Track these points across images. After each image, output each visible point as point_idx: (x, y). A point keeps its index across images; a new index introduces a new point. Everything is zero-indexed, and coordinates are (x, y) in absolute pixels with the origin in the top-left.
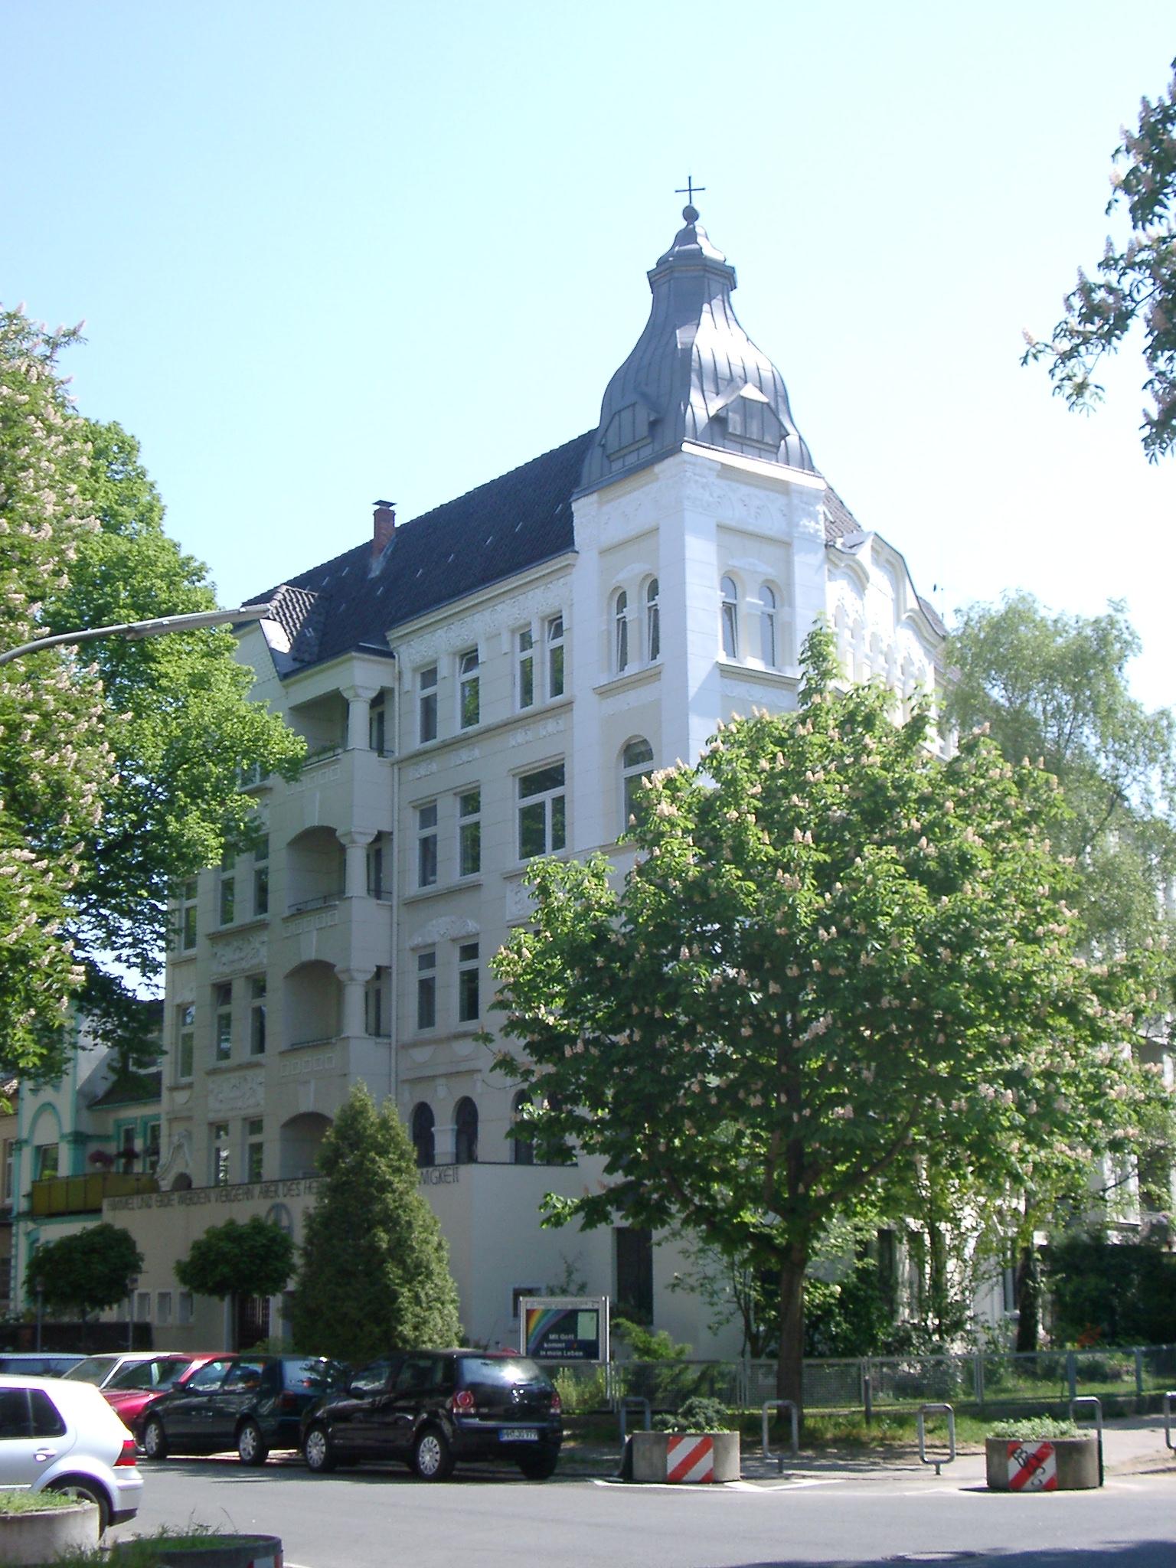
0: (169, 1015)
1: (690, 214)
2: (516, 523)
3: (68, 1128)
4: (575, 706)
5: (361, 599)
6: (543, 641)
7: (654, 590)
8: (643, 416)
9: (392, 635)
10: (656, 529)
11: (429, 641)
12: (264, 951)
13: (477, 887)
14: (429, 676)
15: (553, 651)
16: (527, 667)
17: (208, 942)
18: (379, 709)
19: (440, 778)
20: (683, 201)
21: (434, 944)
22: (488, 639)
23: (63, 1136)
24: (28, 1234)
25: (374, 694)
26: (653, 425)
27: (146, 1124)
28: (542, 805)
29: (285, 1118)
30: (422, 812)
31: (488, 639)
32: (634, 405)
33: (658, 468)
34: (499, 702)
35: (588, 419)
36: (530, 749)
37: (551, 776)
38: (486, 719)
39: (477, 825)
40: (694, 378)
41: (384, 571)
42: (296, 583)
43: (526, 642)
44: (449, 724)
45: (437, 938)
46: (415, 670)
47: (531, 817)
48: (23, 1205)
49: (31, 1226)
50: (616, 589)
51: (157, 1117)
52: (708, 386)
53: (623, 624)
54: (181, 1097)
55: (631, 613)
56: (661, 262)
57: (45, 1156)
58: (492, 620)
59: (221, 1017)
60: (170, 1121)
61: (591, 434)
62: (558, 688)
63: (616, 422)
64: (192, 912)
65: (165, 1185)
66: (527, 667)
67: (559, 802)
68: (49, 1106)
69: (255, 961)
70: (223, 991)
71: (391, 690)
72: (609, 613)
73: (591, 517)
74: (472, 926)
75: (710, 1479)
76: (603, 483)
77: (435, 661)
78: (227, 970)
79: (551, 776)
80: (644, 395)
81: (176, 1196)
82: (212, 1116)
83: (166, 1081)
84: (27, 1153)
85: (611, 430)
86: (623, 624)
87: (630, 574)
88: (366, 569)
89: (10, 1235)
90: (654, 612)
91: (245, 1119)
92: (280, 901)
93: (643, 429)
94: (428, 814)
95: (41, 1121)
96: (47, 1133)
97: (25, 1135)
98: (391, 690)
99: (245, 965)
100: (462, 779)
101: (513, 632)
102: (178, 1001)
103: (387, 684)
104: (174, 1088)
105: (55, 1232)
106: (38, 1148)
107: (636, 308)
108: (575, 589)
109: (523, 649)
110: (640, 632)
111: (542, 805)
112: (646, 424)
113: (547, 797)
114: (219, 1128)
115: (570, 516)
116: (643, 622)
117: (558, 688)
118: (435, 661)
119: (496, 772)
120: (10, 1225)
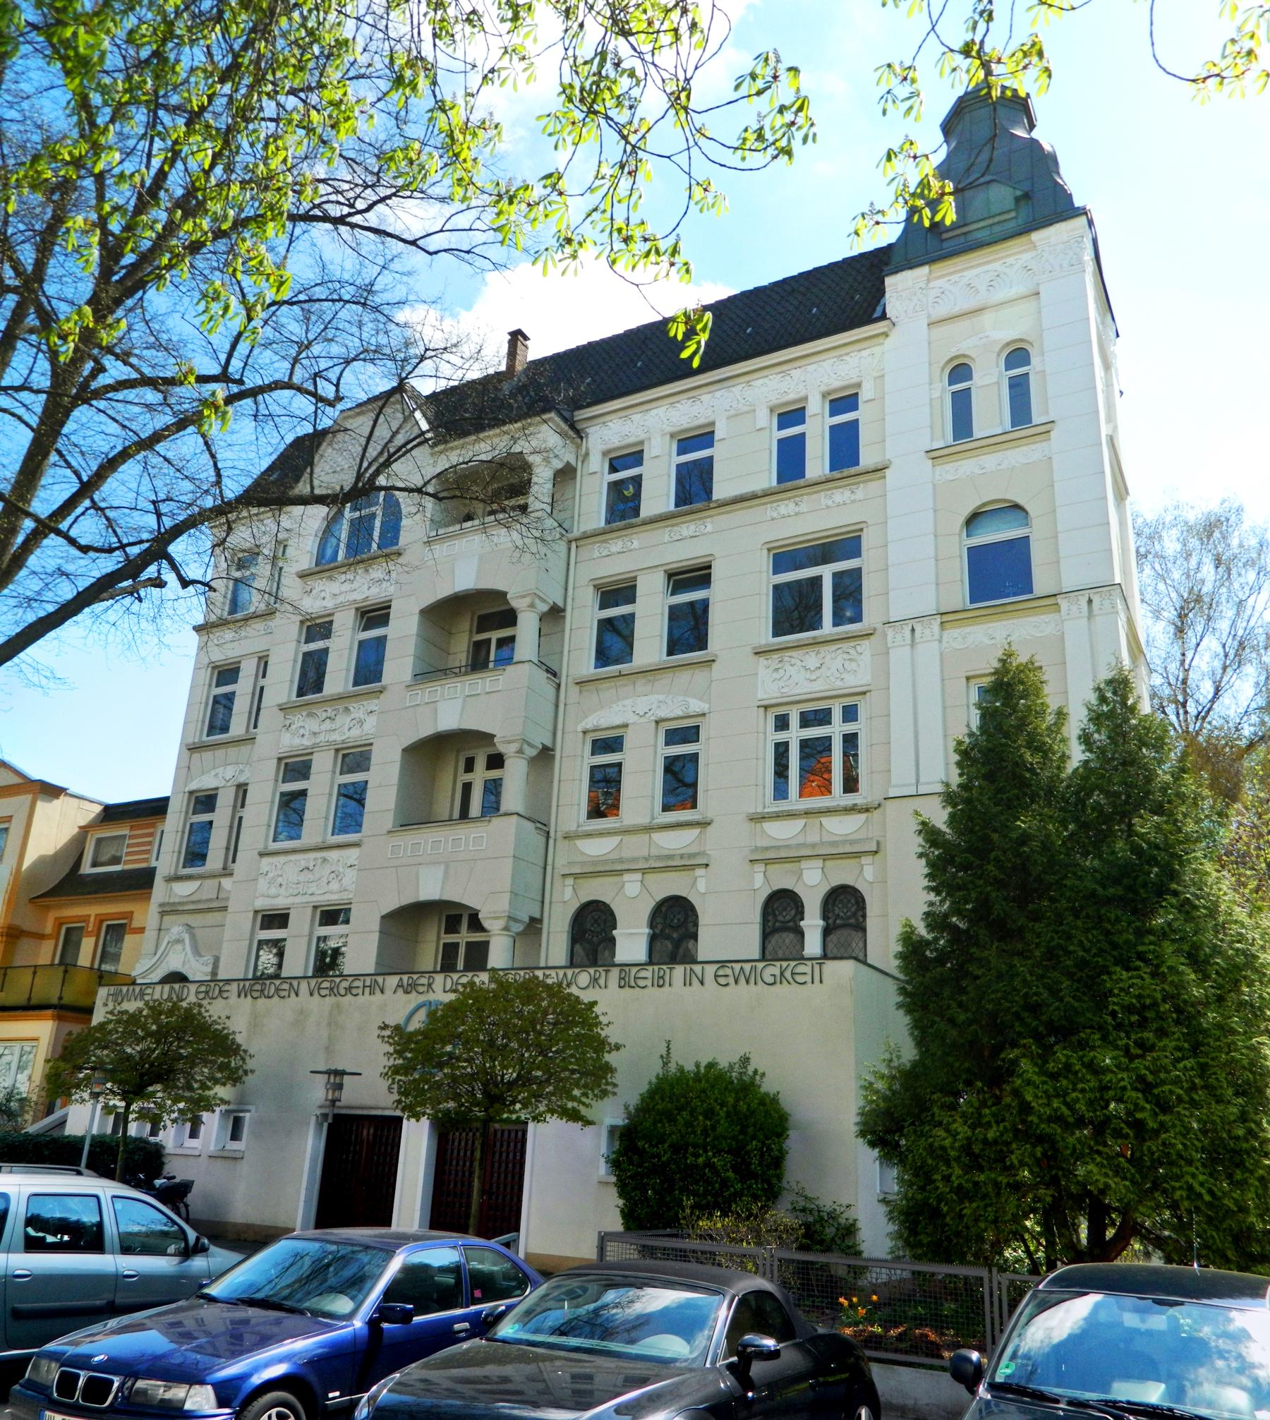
33: (1036, 236)
45: (631, 719)
46: (604, 454)
69: (356, 732)
74: (696, 706)
78: (307, 742)
99: (337, 737)
102: (193, 786)
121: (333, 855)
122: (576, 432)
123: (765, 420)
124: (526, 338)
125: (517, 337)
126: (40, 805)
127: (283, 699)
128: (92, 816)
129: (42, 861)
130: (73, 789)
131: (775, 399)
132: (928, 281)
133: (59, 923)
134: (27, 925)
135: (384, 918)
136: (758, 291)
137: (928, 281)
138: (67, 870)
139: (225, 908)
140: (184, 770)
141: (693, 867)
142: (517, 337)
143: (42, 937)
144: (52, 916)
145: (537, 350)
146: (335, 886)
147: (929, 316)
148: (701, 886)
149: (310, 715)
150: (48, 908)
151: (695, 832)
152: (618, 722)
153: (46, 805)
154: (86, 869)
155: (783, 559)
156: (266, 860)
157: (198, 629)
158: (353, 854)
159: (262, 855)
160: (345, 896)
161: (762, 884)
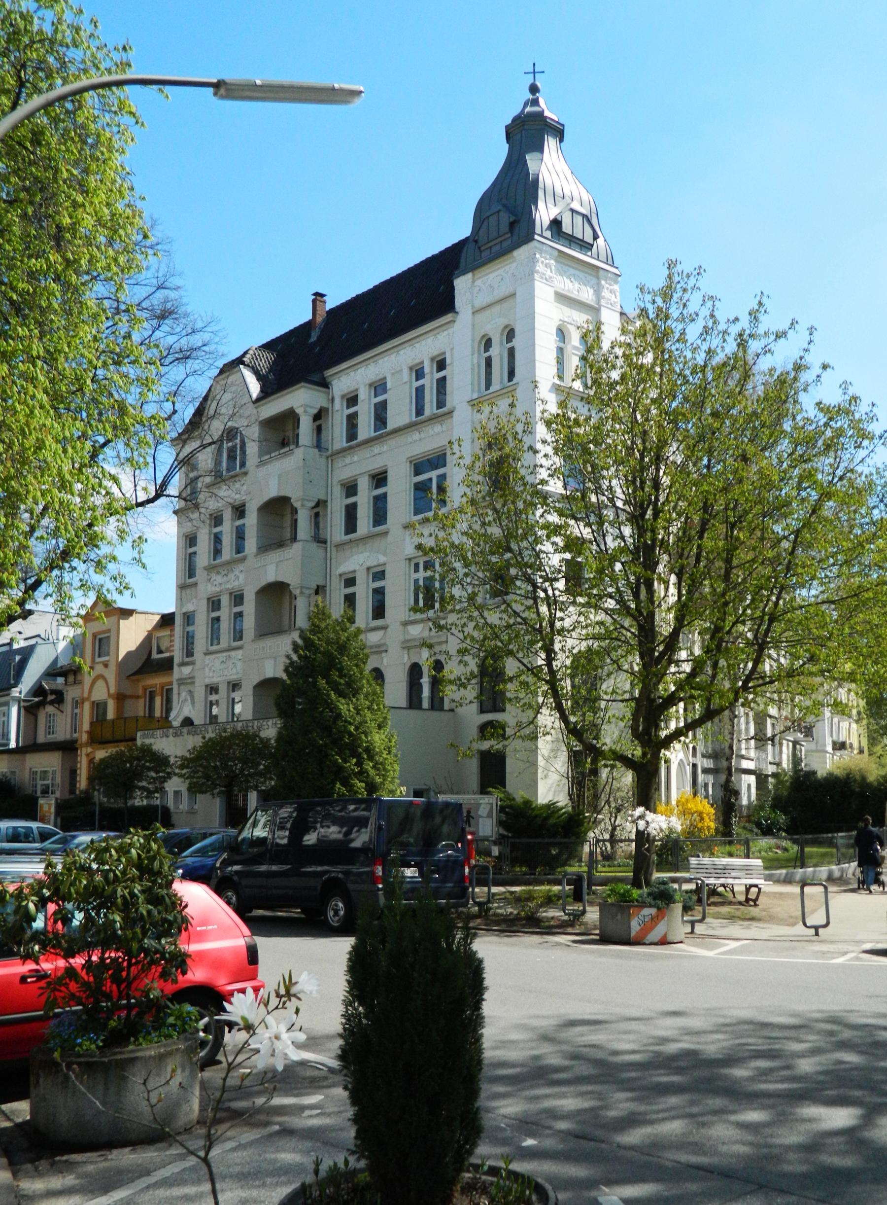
0: (178, 620)
1: (534, 89)
2: (419, 296)
3: (113, 690)
4: (455, 414)
5: (303, 355)
6: (432, 373)
7: (510, 334)
8: (505, 218)
9: (328, 373)
10: (513, 295)
11: (353, 377)
12: (242, 577)
13: (385, 533)
14: (352, 400)
15: (439, 380)
16: (420, 391)
17: (205, 572)
18: (318, 423)
19: (358, 466)
20: (529, 79)
21: (355, 571)
22: (393, 374)
23: (110, 695)
24: (87, 755)
25: (315, 411)
26: (512, 225)
27: (163, 688)
28: (431, 480)
29: (255, 683)
30: (348, 488)
31: (393, 374)
32: (498, 212)
33: (516, 253)
34: (400, 413)
35: (462, 229)
36: (424, 442)
37: (438, 460)
38: (391, 426)
39: (385, 496)
40: (541, 194)
41: (319, 338)
42: (268, 346)
43: (419, 374)
44: (365, 429)
45: (357, 568)
46: (343, 397)
47: (421, 488)
48: (85, 737)
49: (89, 750)
50: (483, 336)
51: (171, 683)
52: (550, 200)
53: (489, 362)
54: (186, 670)
55: (494, 351)
56: (515, 120)
57: (99, 708)
58: (393, 364)
59: (213, 619)
60: (179, 685)
61: (467, 238)
62: (441, 404)
63: (486, 223)
64: (104, 642)
65: (176, 724)
66: (420, 391)
67: (443, 477)
68: (101, 677)
69: (236, 583)
70: (214, 604)
71: (327, 410)
72: (479, 354)
73: (466, 288)
74: (382, 559)
75: (664, 942)
76: (475, 266)
77: (357, 390)
78: (218, 589)
79: (438, 460)
80: (504, 206)
81: (185, 730)
82: (207, 681)
83: (177, 661)
84: (87, 706)
85: (481, 232)
86: (489, 362)
87: (493, 326)
88: (309, 336)
89: (76, 756)
90: (511, 352)
91: (229, 683)
92: (251, 544)
93: (504, 227)
94: (351, 489)
95: (96, 686)
96: (100, 693)
97: (86, 695)
98: (327, 410)
99: (229, 586)
100: (375, 465)
101: (411, 369)
102: (184, 610)
103: (325, 405)
104: (183, 664)
105: (101, 754)
106: (93, 702)
107: (500, 151)
108: (453, 339)
109: (417, 380)
110: (502, 365)
111: (431, 480)
112: (507, 224)
113: (433, 475)
114: (213, 689)
115: (452, 288)
116: (503, 359)
117: (441, 404)
118: (357, 390)
119: (396, 459)
120: (76, 749)
121: (233, 653)
122: (325, 384)
123: (406, 375)
124: (323, 295)
125: (318, 296)
126: (122, 623)
127: (206, 563)
128: (155, 622)
129: (129, 654)
130: (140, 609)
131: (411, 363)
132: (473, 282)
133: (145, 690)
134: (129, 691)
135: (255, 687)
136: (434, 258)
137: (473, 282)
138: (145, 657)
139: (193, 683)
140: (180, 600)
141: (381, 652)
142: (318, 296)
143: (138, 697)
144: (141, 685)
145: (332, 302)
146: (234, 671)
147: (473, 306)
148: (385, 662)
149: (218, 573)
150: (138, 681)
151: (382, 633)
152: (351, 569)
153: (126, 622)
154: (155, 656)
155: (418, 469)
156: (208, 657)
157: (175, 512)
158: (240, 652)
159: (205, 654)
160: (240, 676)
161: (406, 660)
